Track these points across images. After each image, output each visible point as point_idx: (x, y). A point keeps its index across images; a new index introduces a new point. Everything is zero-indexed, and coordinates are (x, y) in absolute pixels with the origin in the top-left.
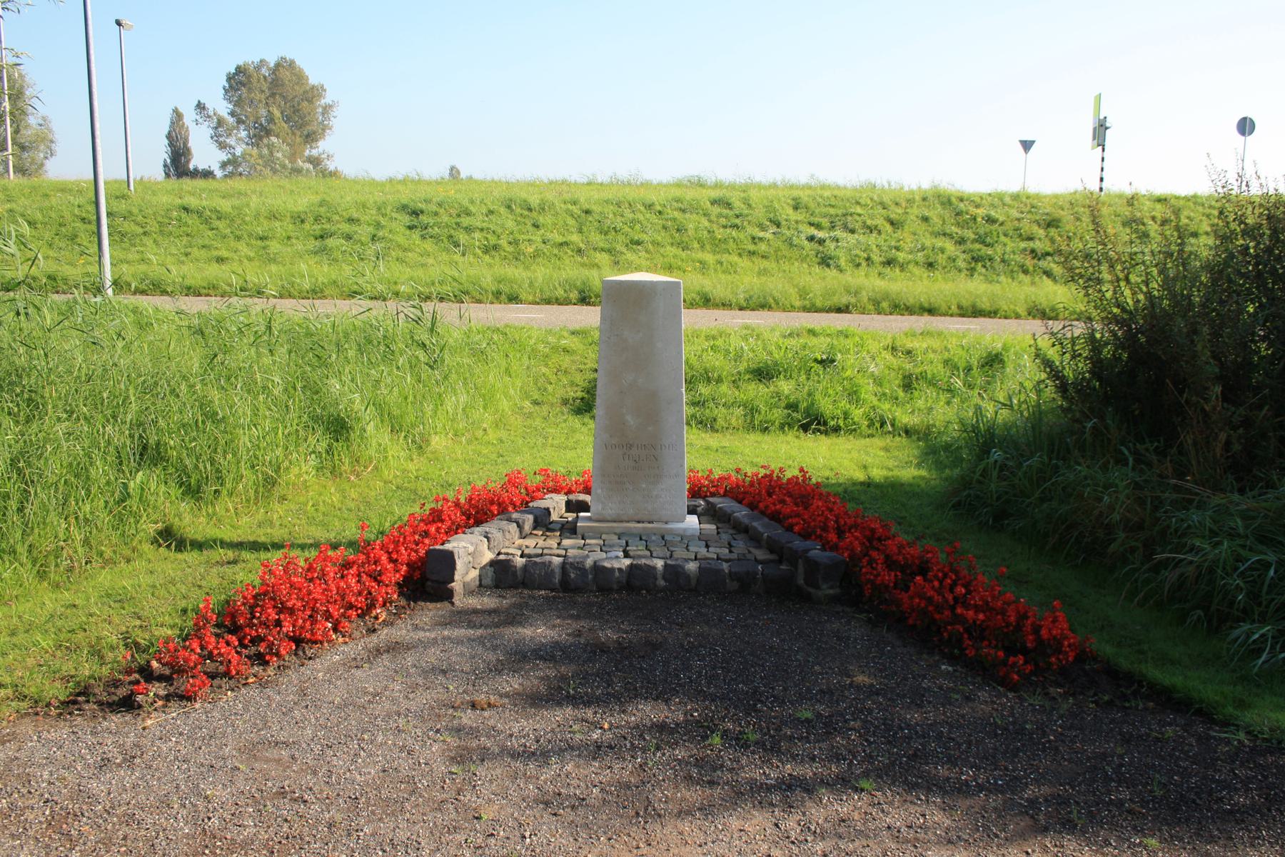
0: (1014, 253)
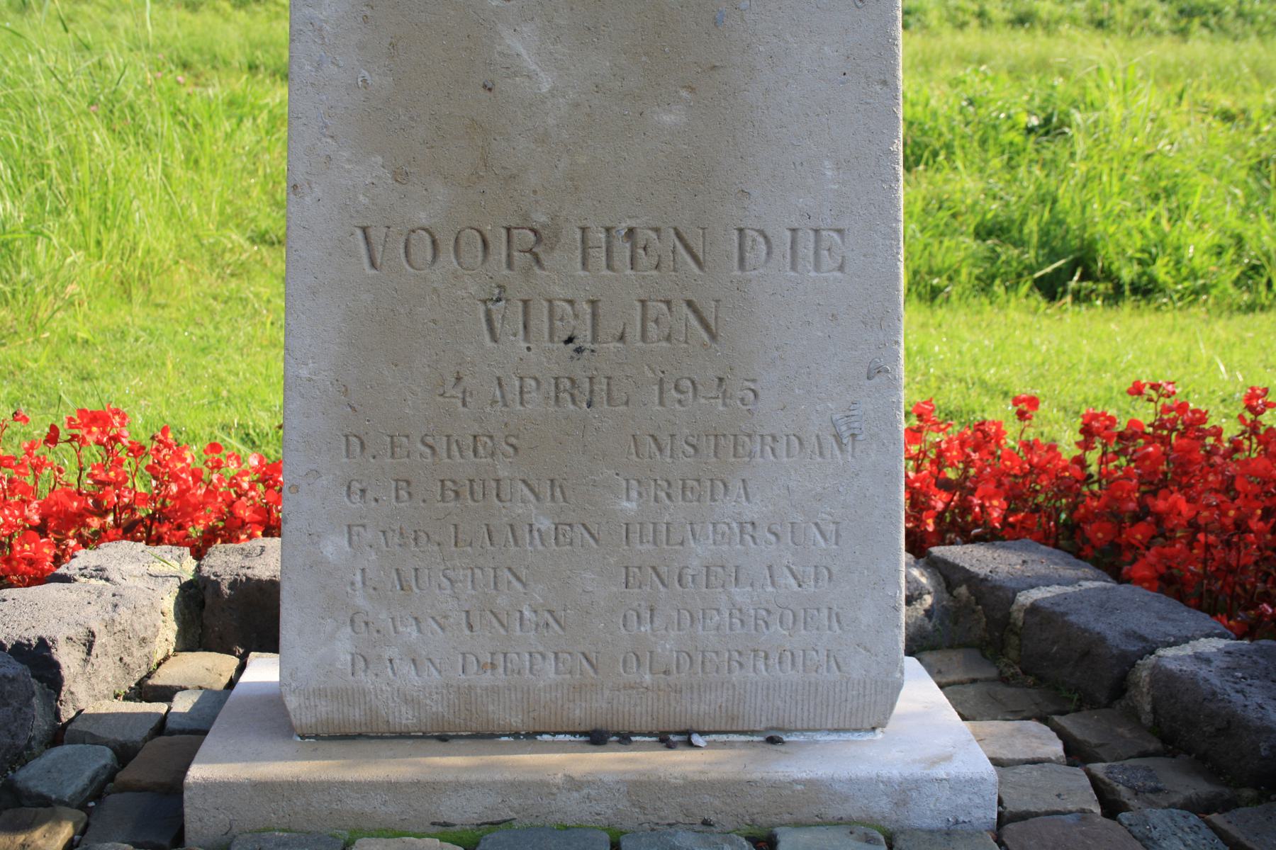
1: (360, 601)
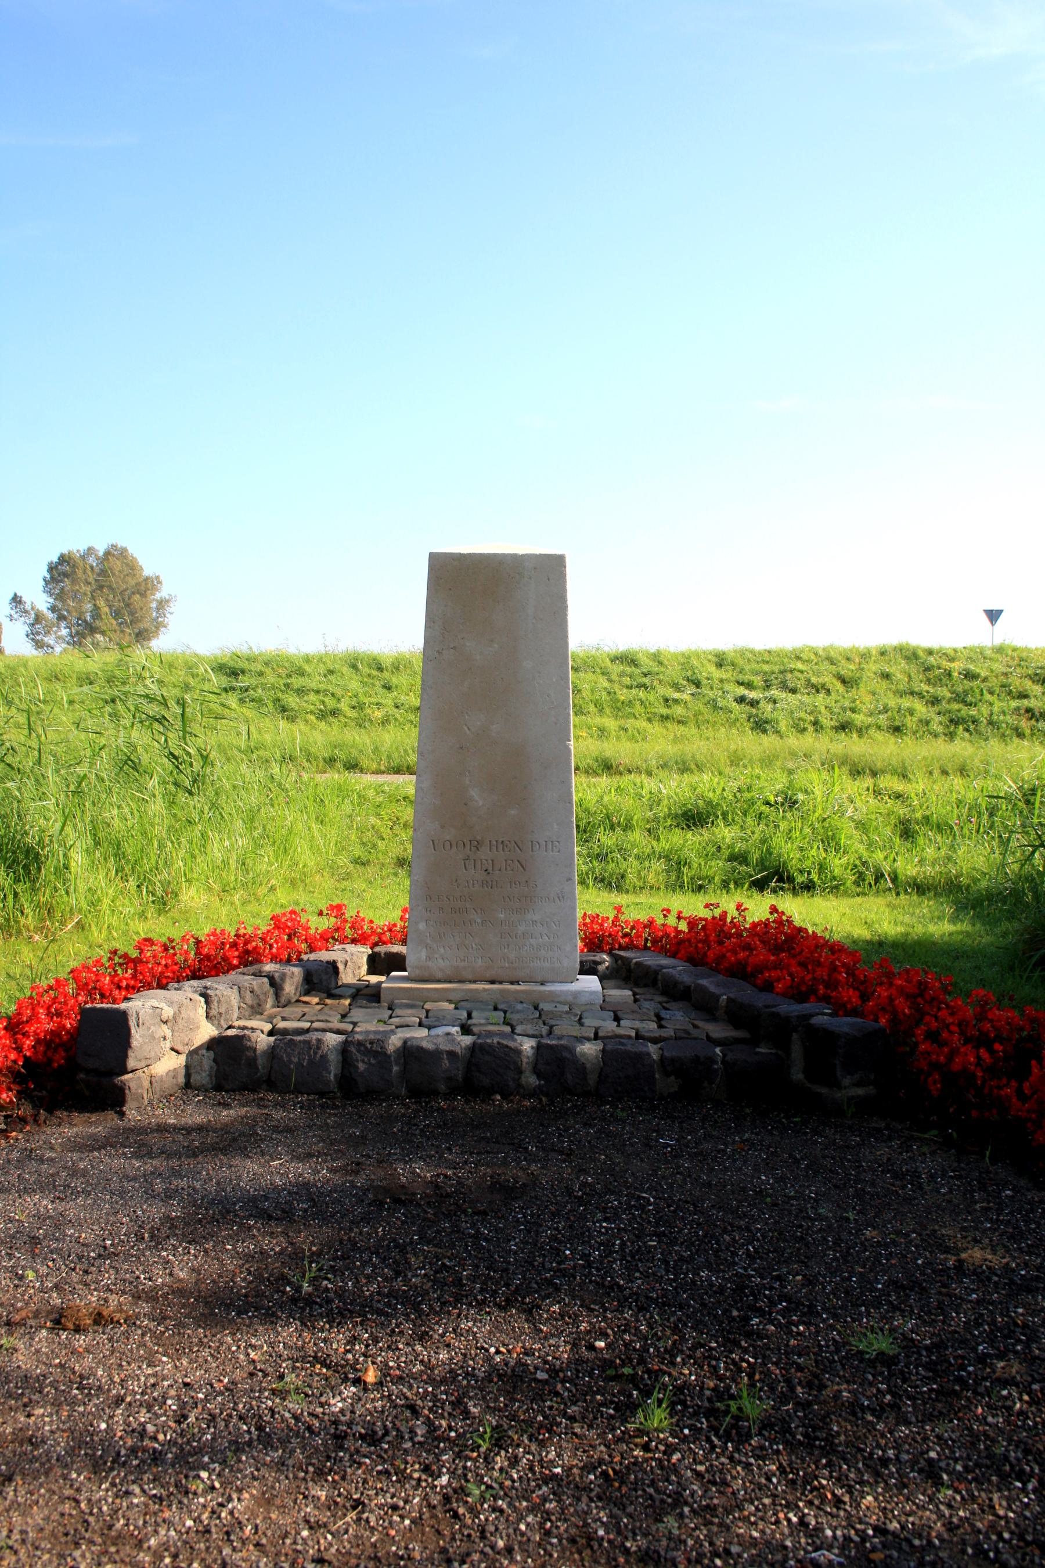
0: (1004, 713)
1: (429, 941)
